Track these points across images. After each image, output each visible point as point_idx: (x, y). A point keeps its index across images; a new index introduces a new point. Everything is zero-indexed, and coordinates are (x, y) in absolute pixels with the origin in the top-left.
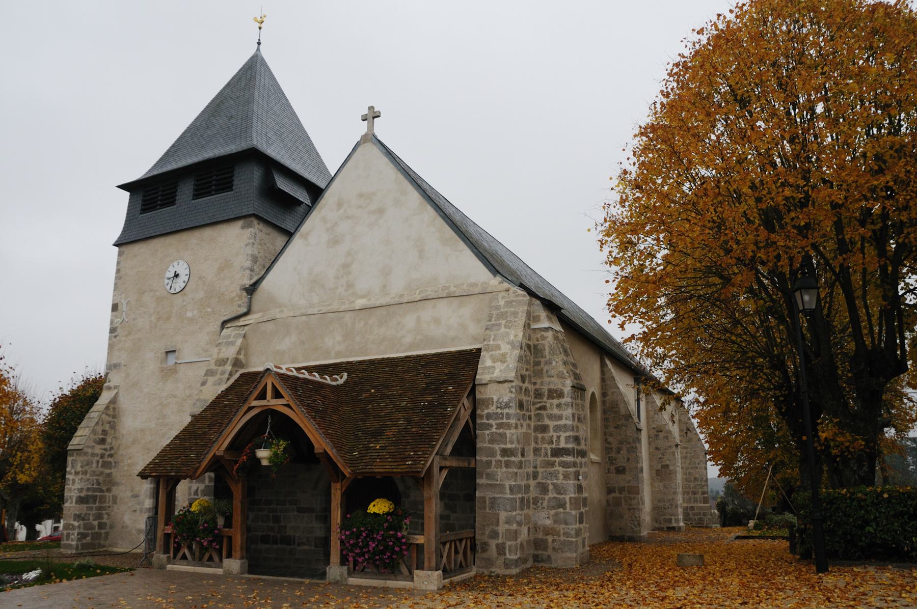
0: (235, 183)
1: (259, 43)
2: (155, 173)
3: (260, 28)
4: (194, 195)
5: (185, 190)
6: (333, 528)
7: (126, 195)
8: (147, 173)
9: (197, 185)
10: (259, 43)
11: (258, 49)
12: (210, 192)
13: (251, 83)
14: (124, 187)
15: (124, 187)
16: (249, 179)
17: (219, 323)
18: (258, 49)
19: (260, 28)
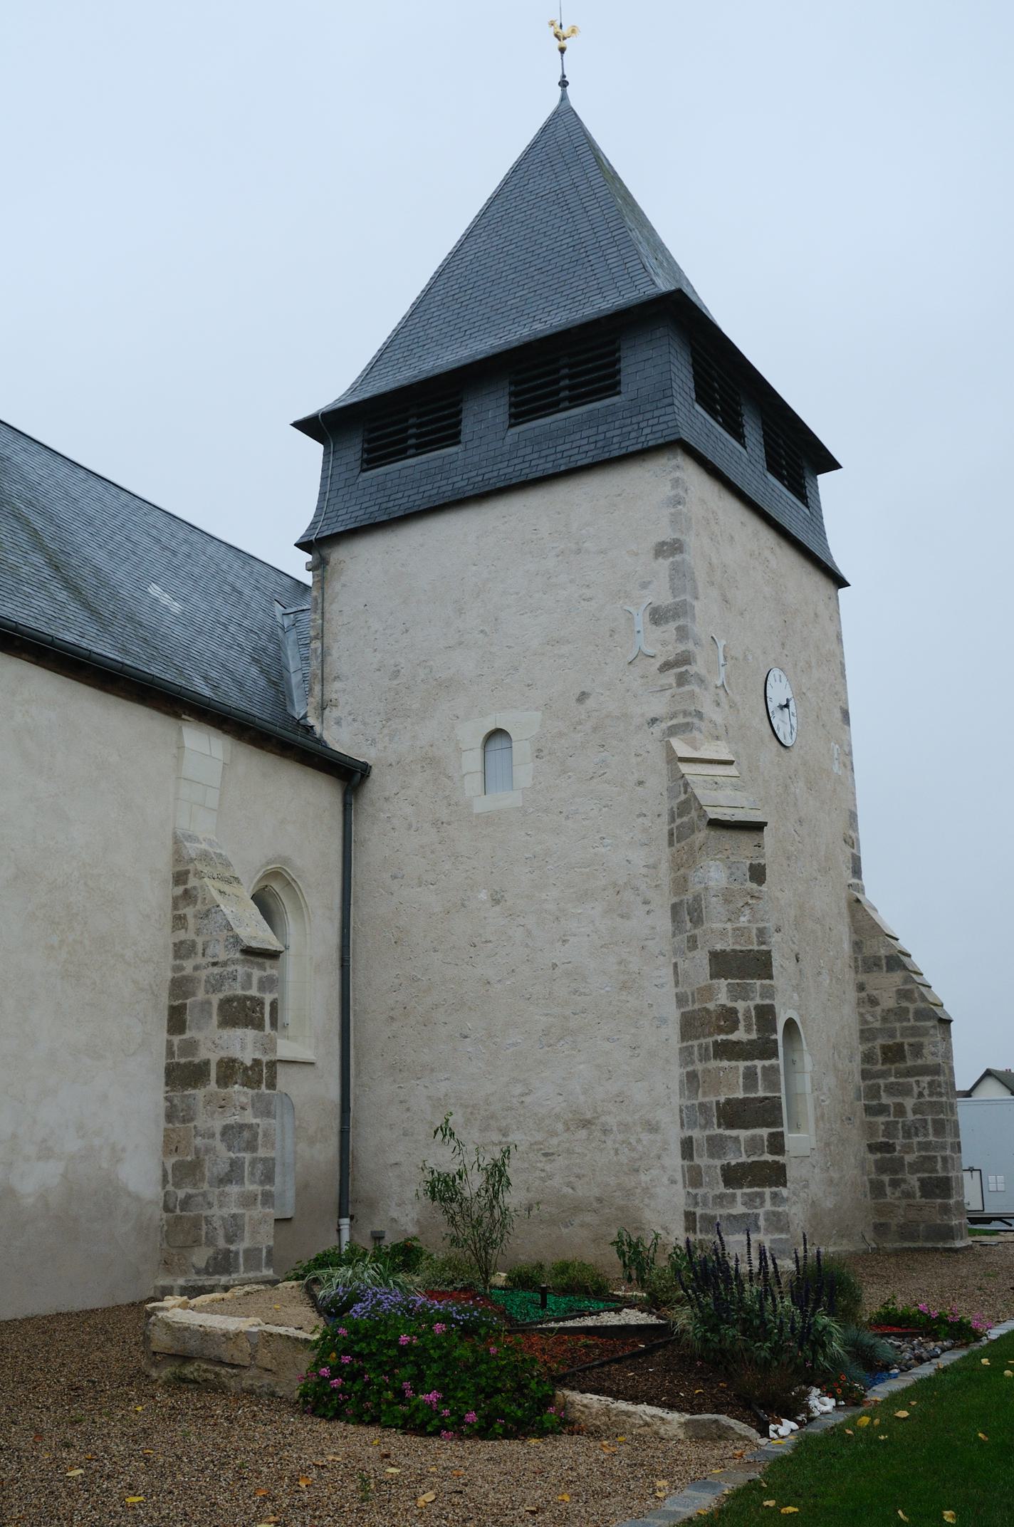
0: (624, 377)
1: (564, 84)
2: (342, 404)
3: (562, 50)
4: (364, 461)
5: (485, 417)
6: (204, 1315)
7: (313, 450)
8: (353, 389)
9: (369, 441)
10: (564, 84)
11: (564, 98)
12: (404, 450)
13: (563, 175)
14: (308, 426)
15: (308, 426)
16: (658, 368)
17: (481, 739)
18: (564, 98)
19: (562, 50)
